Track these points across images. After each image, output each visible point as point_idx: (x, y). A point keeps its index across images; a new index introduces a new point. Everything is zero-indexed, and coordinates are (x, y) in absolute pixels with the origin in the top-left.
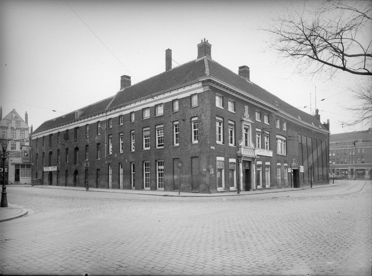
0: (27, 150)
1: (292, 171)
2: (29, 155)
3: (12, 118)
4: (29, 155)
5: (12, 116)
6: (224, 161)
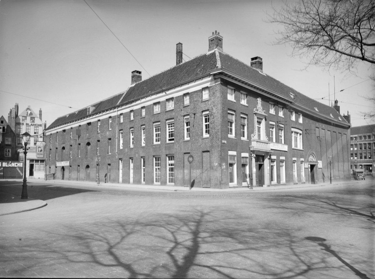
0: (41, 145)
1: (309, 166)
2: (43, 151)
3: (27, 115)
4: (43, 151)
5: (28, 113)
6: (236, 155)
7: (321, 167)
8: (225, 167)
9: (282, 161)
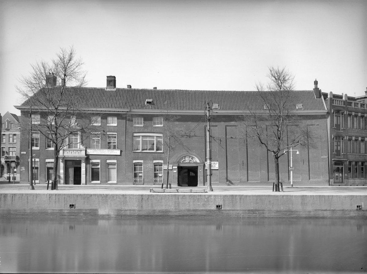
7: (218, 168)
8: (24, 169)
9: (113, 164)
